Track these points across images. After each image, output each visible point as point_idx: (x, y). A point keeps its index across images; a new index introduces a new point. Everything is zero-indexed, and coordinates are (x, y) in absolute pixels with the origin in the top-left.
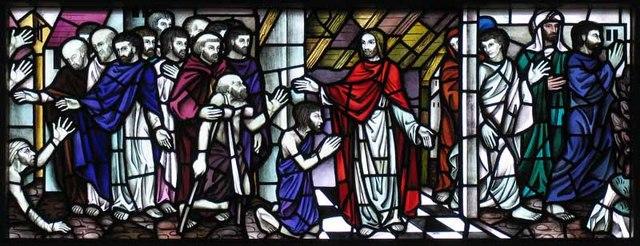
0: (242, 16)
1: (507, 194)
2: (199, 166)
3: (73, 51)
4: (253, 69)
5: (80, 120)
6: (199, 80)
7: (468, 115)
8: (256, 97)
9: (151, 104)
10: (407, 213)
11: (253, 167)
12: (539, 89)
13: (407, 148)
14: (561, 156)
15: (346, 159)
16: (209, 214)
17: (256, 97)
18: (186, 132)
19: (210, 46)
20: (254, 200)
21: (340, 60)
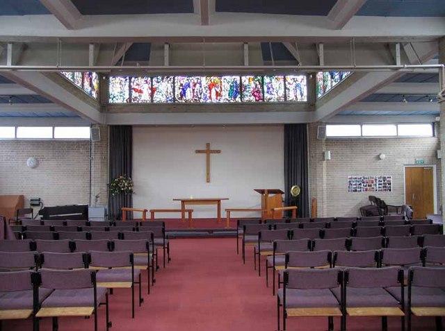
0: (230, 230)
1: (227, 97)
2: (195, 94)
3: (182, 82)
4: (200, 83)
5: (183, 89)
6: (195, 85)
7: (223, 89)
8: (201, 87)
9: (189, 87)
10: (217, 99)
11: (201, 94)
12: (231, 86)
13: (217, 92)
14: (295, 89)
15: (210, 93)
16: (32, 317)
17: (201, 87)
18: (194, 90)
19: (196, 81)
20: (200, 98)
21: (210, 82)
